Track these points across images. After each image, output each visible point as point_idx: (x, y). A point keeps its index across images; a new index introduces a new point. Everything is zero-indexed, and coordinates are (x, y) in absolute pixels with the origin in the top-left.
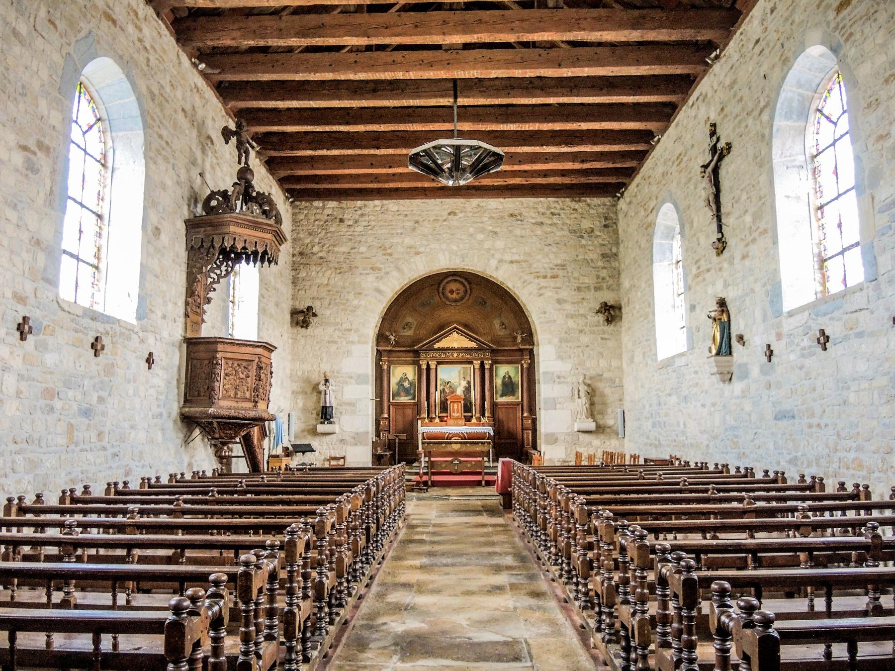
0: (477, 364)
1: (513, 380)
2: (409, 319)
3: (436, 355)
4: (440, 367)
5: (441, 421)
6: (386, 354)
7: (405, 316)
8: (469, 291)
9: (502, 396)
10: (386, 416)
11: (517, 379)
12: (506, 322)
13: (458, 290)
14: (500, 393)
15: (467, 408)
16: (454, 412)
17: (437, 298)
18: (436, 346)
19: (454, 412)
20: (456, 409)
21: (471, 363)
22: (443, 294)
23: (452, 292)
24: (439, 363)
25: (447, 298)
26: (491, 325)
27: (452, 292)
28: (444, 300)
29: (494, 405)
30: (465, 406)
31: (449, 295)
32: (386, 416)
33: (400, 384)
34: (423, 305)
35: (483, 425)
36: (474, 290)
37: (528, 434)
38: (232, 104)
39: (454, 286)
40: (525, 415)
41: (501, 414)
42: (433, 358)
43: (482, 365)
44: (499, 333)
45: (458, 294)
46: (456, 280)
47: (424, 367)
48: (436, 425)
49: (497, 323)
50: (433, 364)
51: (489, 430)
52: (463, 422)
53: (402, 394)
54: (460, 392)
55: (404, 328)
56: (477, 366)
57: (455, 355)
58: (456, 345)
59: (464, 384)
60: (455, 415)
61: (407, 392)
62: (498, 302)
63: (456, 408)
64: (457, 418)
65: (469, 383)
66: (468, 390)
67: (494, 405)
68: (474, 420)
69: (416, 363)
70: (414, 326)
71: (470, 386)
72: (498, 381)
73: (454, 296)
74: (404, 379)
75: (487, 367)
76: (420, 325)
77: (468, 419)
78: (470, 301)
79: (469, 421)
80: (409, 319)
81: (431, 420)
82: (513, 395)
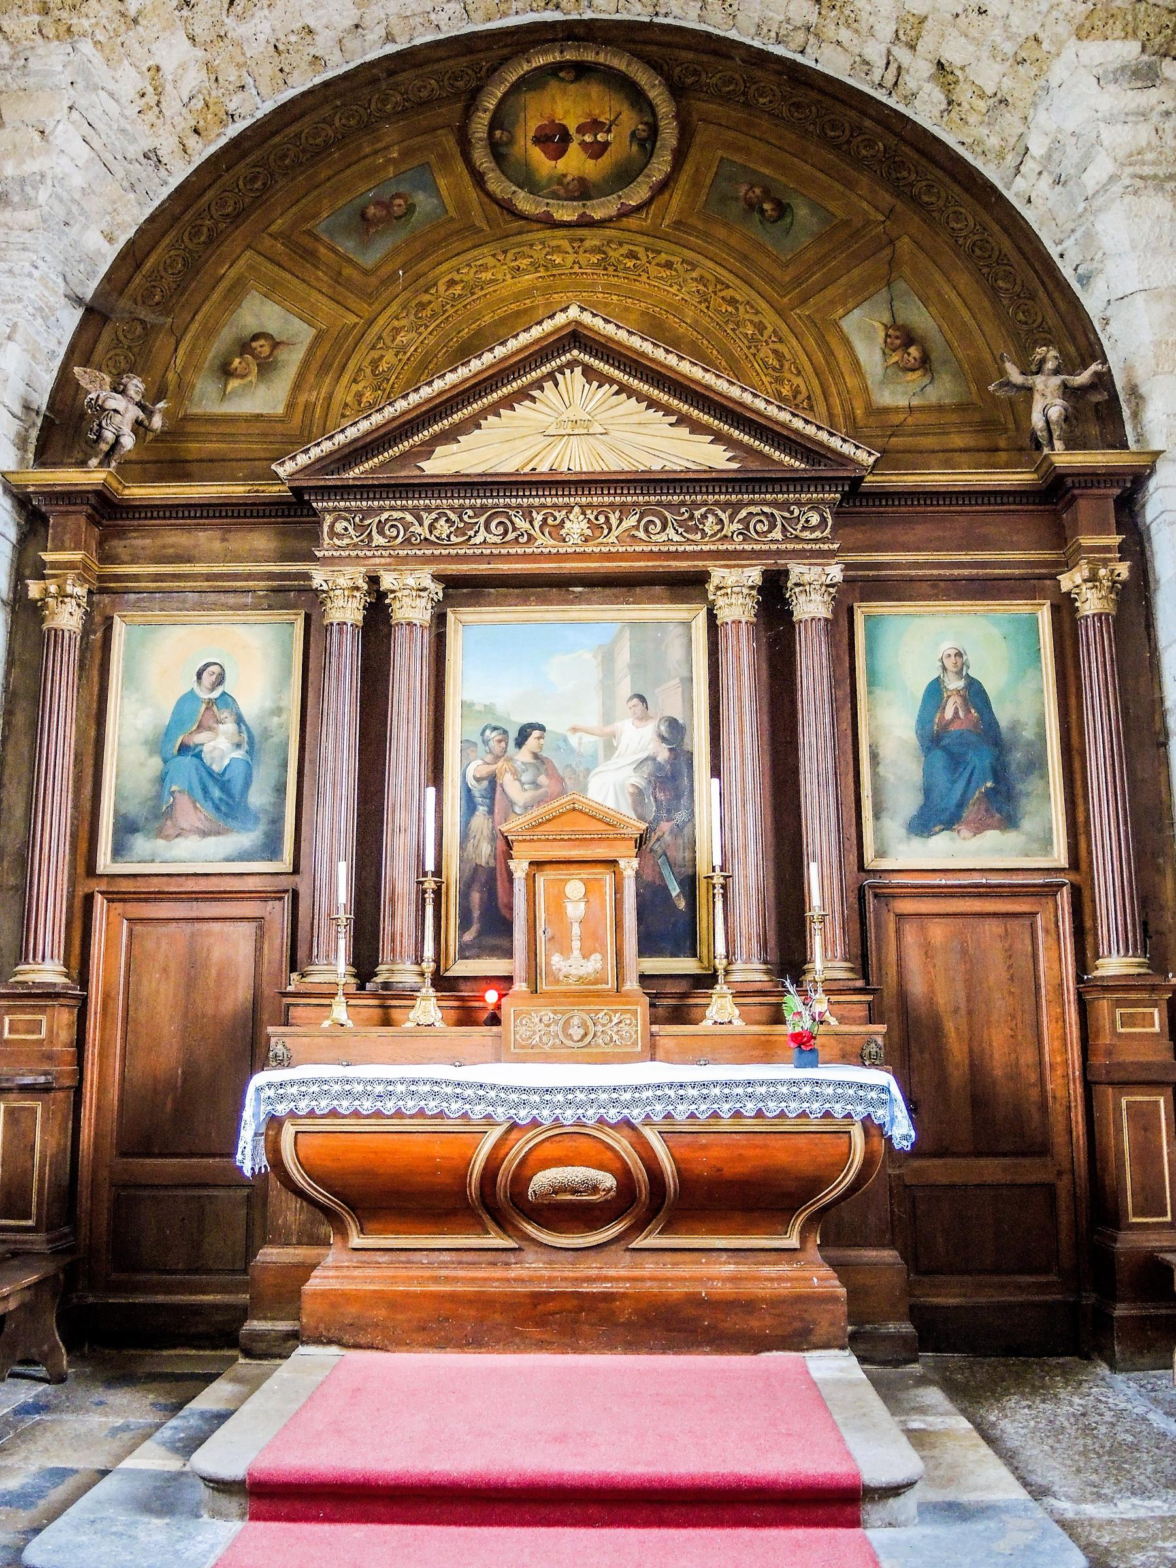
0: (735, 591)
1: (1003, 715)
2: (260, 313)
3: (435, 522)
4: (469, 628)
5: (466, 1016)
6: (78, 522)
7: (235, 294)
8: (669, 135)
9: (926, 822)
10: (48, 971)
11: (1026, 700)
12: (920, 318)
13: (595, 125)
14: (905, 801)
15: (668, 919)
16: (561, 943)
17: (451, 184)
18: (445, 462)
19: (561, 943)
20: (579, 926)
21: (687, 585)
22: (498, 153)
23: (554, 139)
24: (463, 588)
25: (528, 181)
26: (825, 332)
27: (554, 139)
28: (497, 184)
29: (867, 895)
30: (651, 900)
31: (537, 155)
32: (48, 971)
33: (177, 746)
34: (364, 224)
35: (804, 1046)
36: (703, 134)
37: (1144, 1120)
38: (865, 1367)
39: (568, 106)
40: (1114, 964)
41: (924, 961)
42: (412, 551)
43: (773, 595)
44: (886, 397)
45: (597, 150)
46: (581, 71)
47: (347, 611)
48: (420, 1046)
49: (864, 333)
50: (412, 600)
51: (858, 1099)
52: (632, 1019)
53: (189, 814)
54: (612, 788)
55: (226, 371)
56: (737, 608)
57: (576, 526)
58: (578, 458)
59: (640, 740)
60: (572, 965)
61: (224, 799)
62: (866, 201)
63: (575, 910)
64: (586, 994)
65: (675, 732)
66: (670, 780)
67: (867, 895)
68: (720, 1009)
69: (298, 597)
70: (292, 359)
71: (681, 758)
72: (893, 724)
73: (574, 162)
74: (211, 699)
75: (810, 607)
76: (329, 357)
77: (675, 1003)
78: (676, 200)
79: (680, 1015)
80: (260, 313)
81: (387, 1005)
82: (1009, 822)
